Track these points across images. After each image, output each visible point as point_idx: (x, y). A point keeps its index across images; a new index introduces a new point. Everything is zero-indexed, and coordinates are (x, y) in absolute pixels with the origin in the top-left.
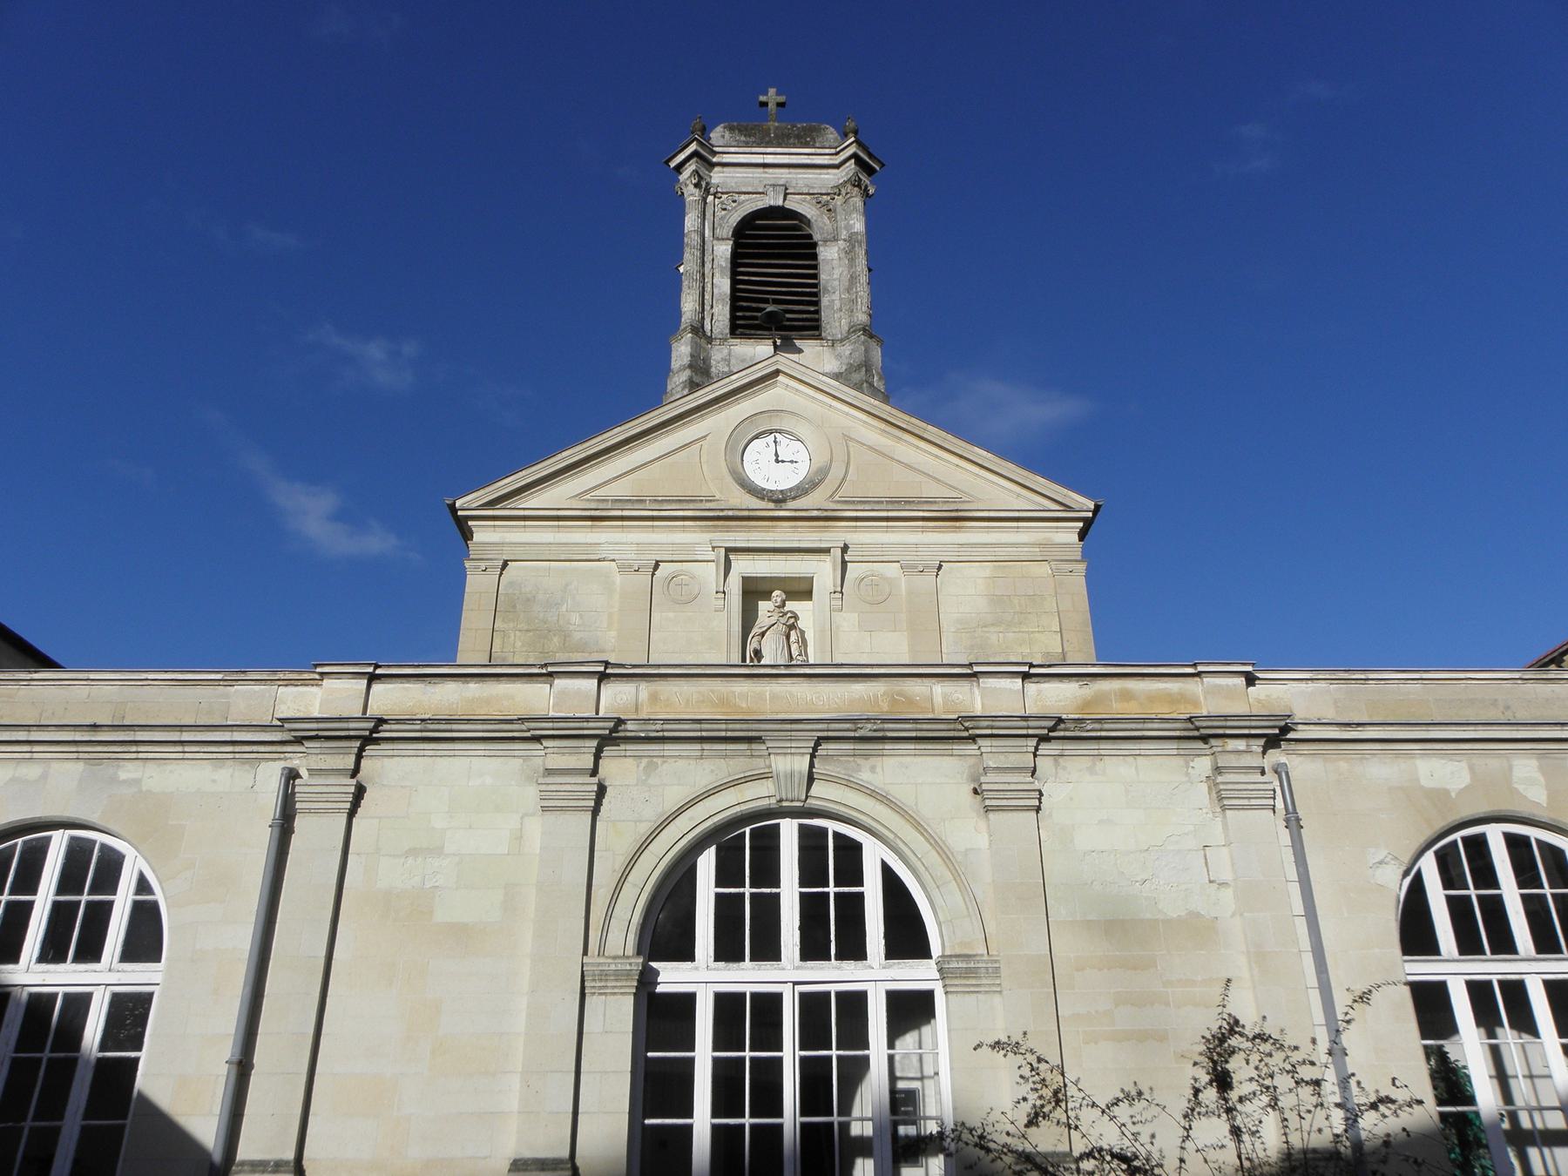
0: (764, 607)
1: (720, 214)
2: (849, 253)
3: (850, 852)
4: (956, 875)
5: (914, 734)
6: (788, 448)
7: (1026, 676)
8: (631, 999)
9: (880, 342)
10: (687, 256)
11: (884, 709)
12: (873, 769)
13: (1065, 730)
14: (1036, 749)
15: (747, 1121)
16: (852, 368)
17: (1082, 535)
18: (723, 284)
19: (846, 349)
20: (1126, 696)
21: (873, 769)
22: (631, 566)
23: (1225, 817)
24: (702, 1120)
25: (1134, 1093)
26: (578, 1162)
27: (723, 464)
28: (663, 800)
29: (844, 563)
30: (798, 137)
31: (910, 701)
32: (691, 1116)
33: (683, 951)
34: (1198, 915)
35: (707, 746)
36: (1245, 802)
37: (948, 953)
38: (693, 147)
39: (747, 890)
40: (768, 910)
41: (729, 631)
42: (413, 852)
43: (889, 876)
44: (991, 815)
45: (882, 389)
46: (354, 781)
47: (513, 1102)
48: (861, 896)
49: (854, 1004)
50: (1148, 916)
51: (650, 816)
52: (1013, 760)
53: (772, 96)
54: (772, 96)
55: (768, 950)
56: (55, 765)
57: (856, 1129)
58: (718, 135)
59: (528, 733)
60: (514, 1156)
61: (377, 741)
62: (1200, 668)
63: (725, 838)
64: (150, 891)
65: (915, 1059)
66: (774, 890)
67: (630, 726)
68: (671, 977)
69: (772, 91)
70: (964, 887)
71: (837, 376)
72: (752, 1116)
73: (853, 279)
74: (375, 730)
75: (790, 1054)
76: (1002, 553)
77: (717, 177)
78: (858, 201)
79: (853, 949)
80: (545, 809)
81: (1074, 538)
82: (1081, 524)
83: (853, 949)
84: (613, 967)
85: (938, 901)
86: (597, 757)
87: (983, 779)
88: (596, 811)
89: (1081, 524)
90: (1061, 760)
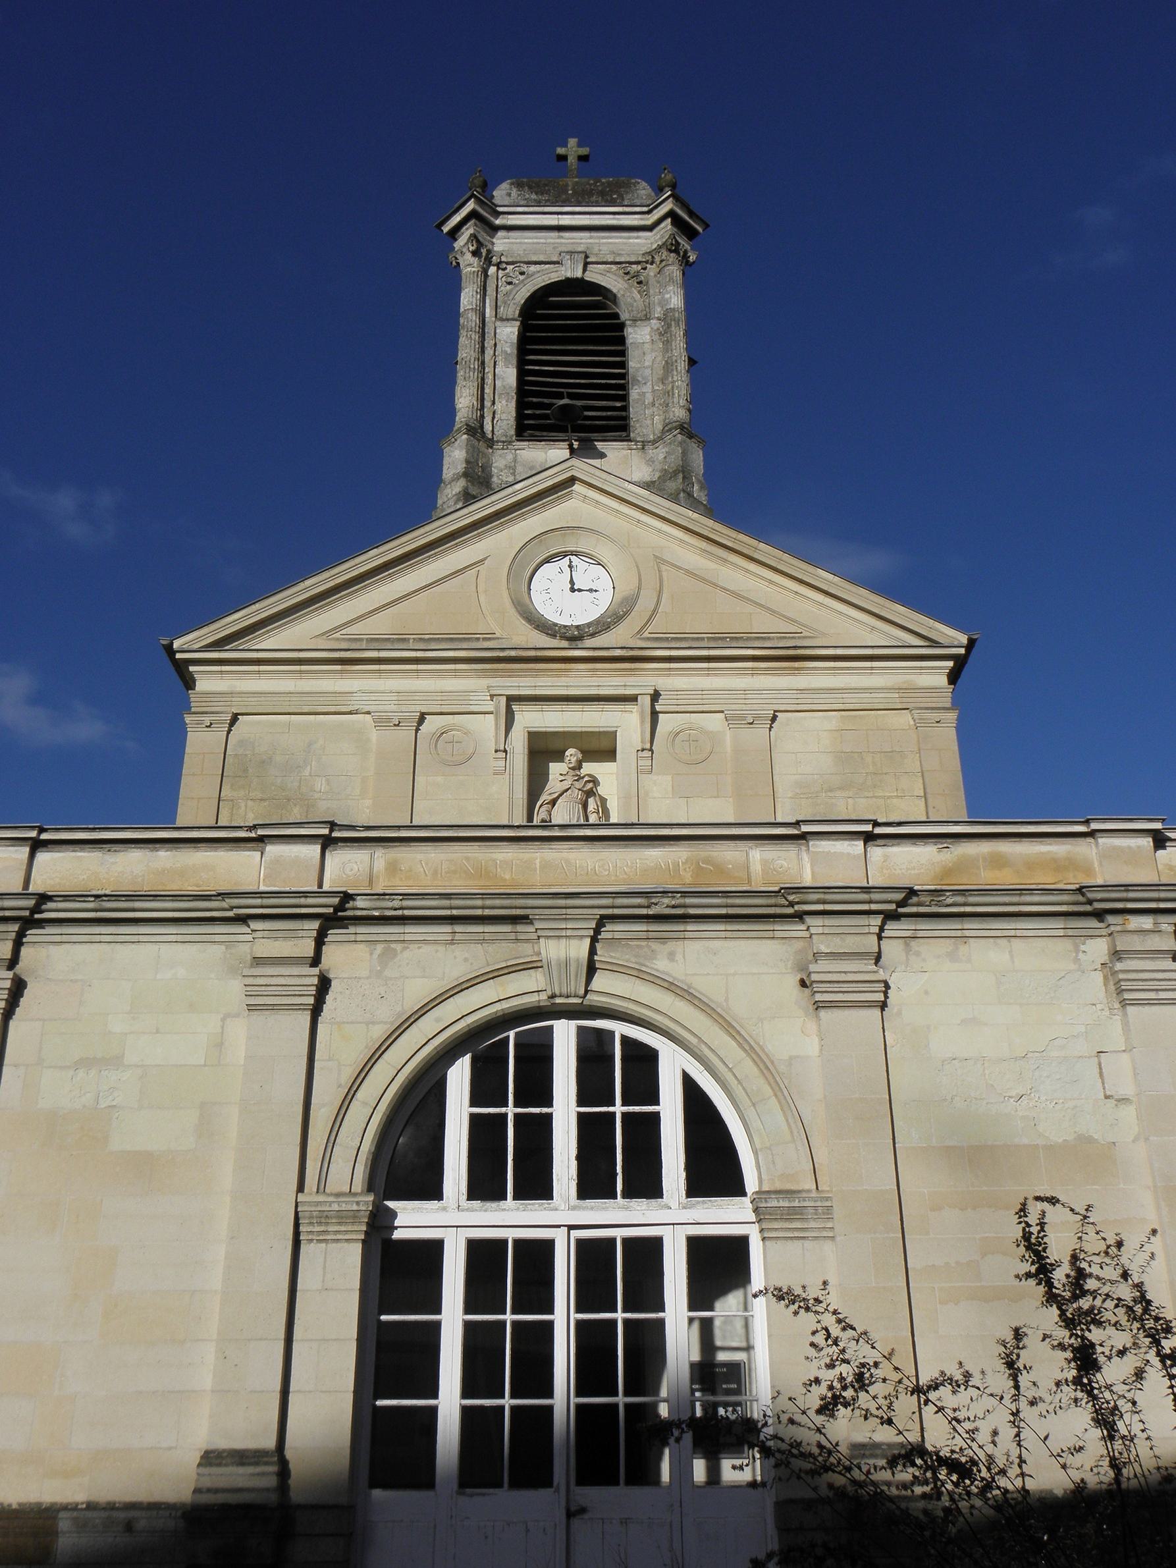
0: (556, 769)
1: (504, 288)
2: (664, 334)
3: (642, 1061)
4: (777, 1089)
5: (723, 911)
6: (586, 573)
7: (869, 838)
8: (358, 1247)
9: (702, 442)
10: (463, 340)
11: (687, 879)
12: (671, 956)
13: (919, 904)
14: (882, 929)
15: (507, 1402)
16: (667, 475)
17: (954, 677)
18: (508, 375)
19: (659, 453)
20: (998, 862)
21: (671, 956)
22: (389, 719)
23: (1125, 1014)
24: (449, 1400)
25: (958, 1376)
26: (289, 1454)
27: (505, 594)
28: (405, 995)
29: (654, 714)
30: (602, 194)
31: (720, 869)
32: (436, 1396)
33: (431, 1190)
34: (1090, 1140)
35: (459, 928)
36: (1152, 995)
37: (766, 1188)
38: (471, 206)
39: (511, 1110)
40: (537, 1134)
41: (511, 799)
42: (86, 1063)
43: (692, 1090)
44: (823, 1013)
45: (704, 500)
46: (10, 974)
47: (205, 1380)
48: (656, 1117)
49: (646, 1252)
50: (1025, 1141)
51: (386, 1016)
52: (850, 944)
53: (572, 148)
54: (572, 148)
55: (535, 1184)
57: (664, 1411)
58: (502, 193)
59: (231, 912)
60: (205, 1446)
61: (41, 923)
62: (1094, 826)
63: (481, 1043)
65: (739, 1324)
66: (545, 1110)
67: (360, 903)
68: (412, 1220)
69: (572, 142)
70: (787, 1103)
71: (648, 486)
72: (513, 1396)
73: (668, 366)
74: (36, 909)
75: (563, 1317)
76: (853, 700)
77: (501, 243)
78: (675, 271)
79: (645, 1184)
80: (251, 1008)
81: (943, 680)
82: (951, 664)
83: (645, 1184)
84: (335, 1207)
85: (755, 1124)
86: (320, 942)
87: (812, 967)
88: (316, 1011)
89: (951, 664)
90: (913, 943)
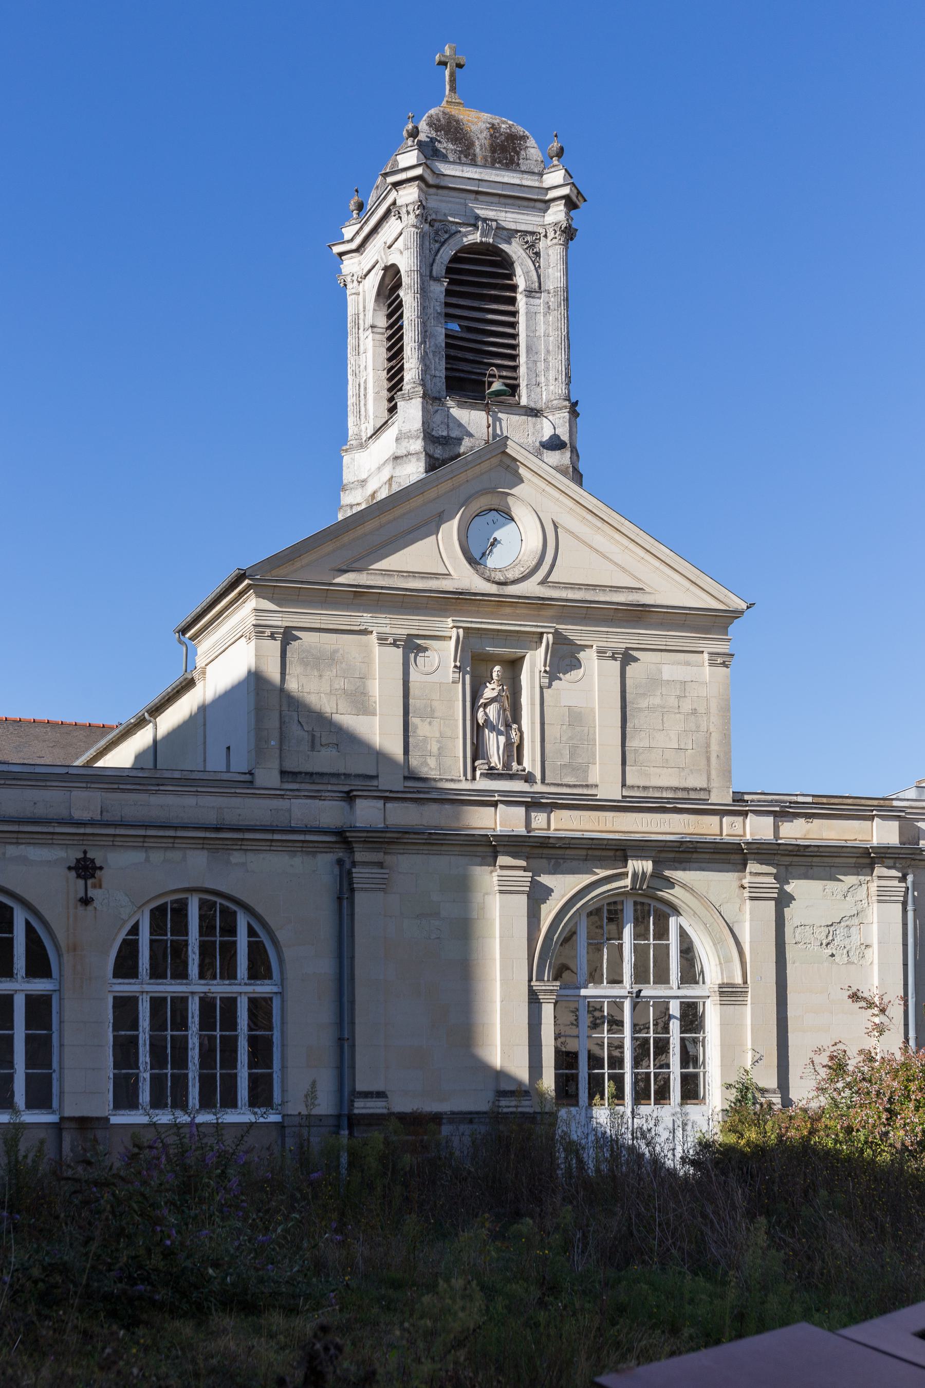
56: (189, 853)
64: (257, 935)
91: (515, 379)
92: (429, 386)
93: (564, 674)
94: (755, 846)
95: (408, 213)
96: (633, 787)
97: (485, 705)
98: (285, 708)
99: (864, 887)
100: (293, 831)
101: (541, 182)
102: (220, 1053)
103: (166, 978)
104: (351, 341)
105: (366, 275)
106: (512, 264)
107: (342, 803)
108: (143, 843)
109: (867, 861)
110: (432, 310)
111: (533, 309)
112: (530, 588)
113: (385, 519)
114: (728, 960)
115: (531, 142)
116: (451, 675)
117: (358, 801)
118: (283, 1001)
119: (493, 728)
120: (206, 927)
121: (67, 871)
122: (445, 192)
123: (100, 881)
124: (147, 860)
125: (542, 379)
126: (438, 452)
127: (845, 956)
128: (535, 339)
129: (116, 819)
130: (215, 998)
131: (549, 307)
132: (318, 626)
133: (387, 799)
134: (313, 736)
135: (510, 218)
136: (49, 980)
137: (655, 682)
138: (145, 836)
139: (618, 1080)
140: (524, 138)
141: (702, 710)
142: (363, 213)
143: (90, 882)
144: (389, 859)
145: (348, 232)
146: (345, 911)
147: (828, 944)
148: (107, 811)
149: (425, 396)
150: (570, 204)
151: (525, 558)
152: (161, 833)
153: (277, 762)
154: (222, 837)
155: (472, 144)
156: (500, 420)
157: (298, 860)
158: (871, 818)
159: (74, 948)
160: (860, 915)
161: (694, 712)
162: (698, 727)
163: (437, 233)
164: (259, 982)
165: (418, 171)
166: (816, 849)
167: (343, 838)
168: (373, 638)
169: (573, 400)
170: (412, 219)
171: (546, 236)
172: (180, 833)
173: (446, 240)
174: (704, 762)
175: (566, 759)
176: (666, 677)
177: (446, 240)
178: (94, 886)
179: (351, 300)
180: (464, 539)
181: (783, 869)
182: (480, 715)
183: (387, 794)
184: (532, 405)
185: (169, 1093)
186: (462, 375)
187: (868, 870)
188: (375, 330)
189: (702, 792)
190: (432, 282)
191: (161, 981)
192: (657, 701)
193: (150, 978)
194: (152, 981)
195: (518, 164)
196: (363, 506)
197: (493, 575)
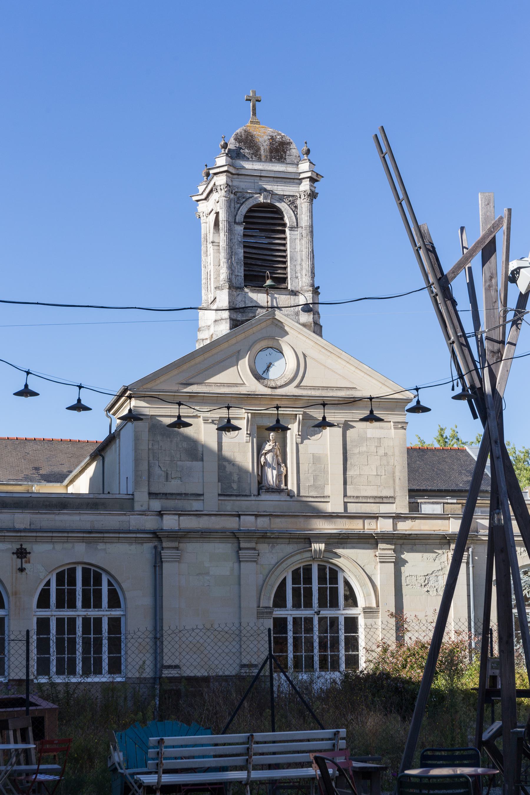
40: (72, 593)
56: (76, 544)
66: (336, 586)
67: (268, 534)
90: (403, 546)
91: (285, 274)
92: (234, 281)
93: (311, 436)
94: (381, 535)
95: (221, 189)
96: (350, 497)
97: (266, 454)
98: (151, 458)
99: (446, 555)
100: (130, 532)
101: (298, 168)
102: (92, 646)
103: (65, 608)
104: (203, 248)
105: (210, 213)
106: (282, 212)
107: (157, 517)
108: (51, 540)
109: (446, 541)
110: (236, 240)
111: (293, 237)
112: (291, 390)
113: (206, 355)
114: (369, 595)
115: (293, 146)
116: (245, 438)
117: (164, 516)
118: (126, 619)
119: (270, 466)
120: (86, 582)
121: (12, 554)
122: (243, 177)
123: (29, 559)
124: (54, 548)
125: (299, 275)
126: (239, 317)
127: (435, 591)
128: (295, 253)
129: (38, 528)
130: (91, 618)
131: (302, 236)
132: (169, 414)
133: (180, 515)
134: (167, 474)
135: (280, 189)
136: (4, 610)
137: (363, 439)
138: (52, 537)
139: (311, 659)
140: (289, 143)
141: (390, 453)
142: (209, 178)
143: (24, 560)
144: (182, 545)
145: (201, 189)
146: (158, 573)
147: (425, 586)
148: (33, 524)
149: (230, 288)
150: (313, 180)
151: (288, 373)
152: (60, 535)
153: (147, 488)
154: (93, 536)
155: (259, 149)
156: (276, 298)
157: (133, 547)
158: (448, 518)
159: (15, 594)
160: (443, 570)
161: (386, 454)
162: (388, 463)
163: (238, 198)
164: (113, 610)
165: (225, 168)
166: (415, 536)
167: (156, 535)
168: (201, 419)
169: (316, 286)
170: (223, 193)
171: (300, 197)
172: (70, 535)
173: (243, 202)
174: (391, 482)
175: (312, 483)
176: (369, 436)
177: (243, 202)
178: (26, 562)
179: (203, 225)
180: (252, 364)
181: (399, 546)
182: (262, 459)
183: (180, 512)
184: (293, 289)
185: (67, 667)
186: (255, 273)
187: (447, 546)
188: (214, 244)
189: (391, 499)
190: (236, 226)
191: (62, 610)
192: (364, 449)
193: (56, 608)
194: (57, 610)
195: (285, 159)
196: (208, 342)
197: (269, 384)
